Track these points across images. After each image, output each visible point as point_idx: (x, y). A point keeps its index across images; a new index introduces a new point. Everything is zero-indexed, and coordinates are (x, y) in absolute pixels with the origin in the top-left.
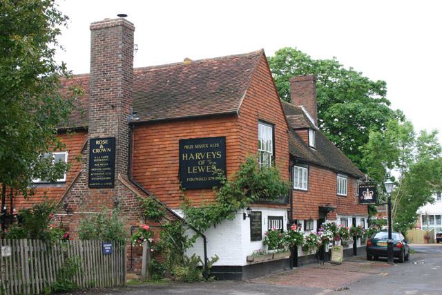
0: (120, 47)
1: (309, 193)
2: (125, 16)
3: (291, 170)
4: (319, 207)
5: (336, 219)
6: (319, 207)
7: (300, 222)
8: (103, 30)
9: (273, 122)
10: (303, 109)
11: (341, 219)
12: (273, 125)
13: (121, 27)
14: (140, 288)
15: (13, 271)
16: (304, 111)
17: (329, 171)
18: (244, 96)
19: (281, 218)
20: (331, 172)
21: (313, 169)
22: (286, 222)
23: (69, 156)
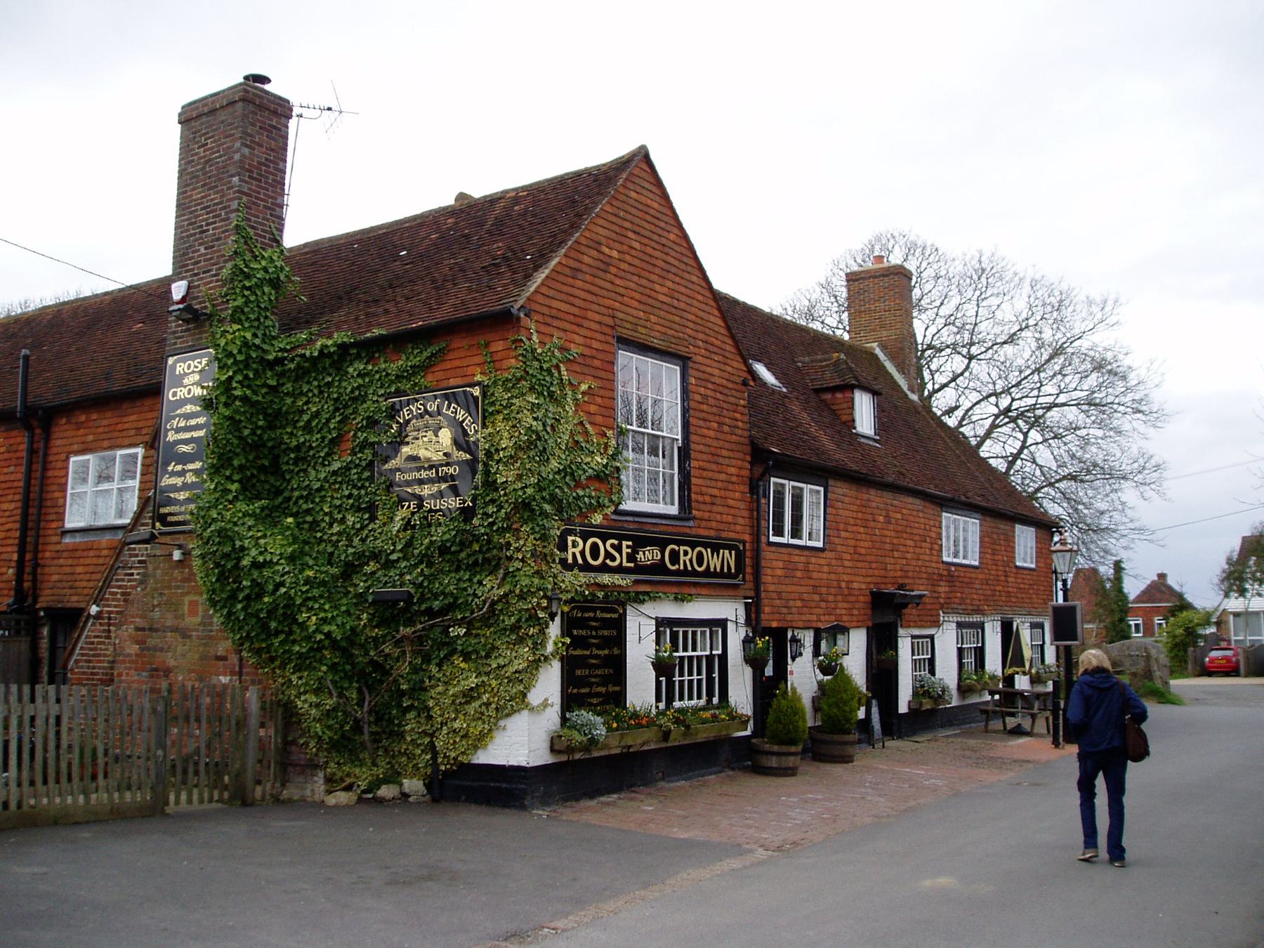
0: (237, 157)
1: (827, 554)
2: (265, 80)
3: (756, 487)
4: (872, 593)
5: (937, 624)
6: (872, 593)
7: (800, 634)
8: (204, 119)
9: (682, 350)
10: (878, 351)
11: (960, 625)
12: (683, 360)
13: (240, 104)
14: (61, 821)
15: (32, 768)
16: (881, 356)
17: (910, 500)
18: (554, 263)
19: (722, 623)
20: (918, 501)
21: (841, 490)
22: (736, 637)
23: (145, 457)
